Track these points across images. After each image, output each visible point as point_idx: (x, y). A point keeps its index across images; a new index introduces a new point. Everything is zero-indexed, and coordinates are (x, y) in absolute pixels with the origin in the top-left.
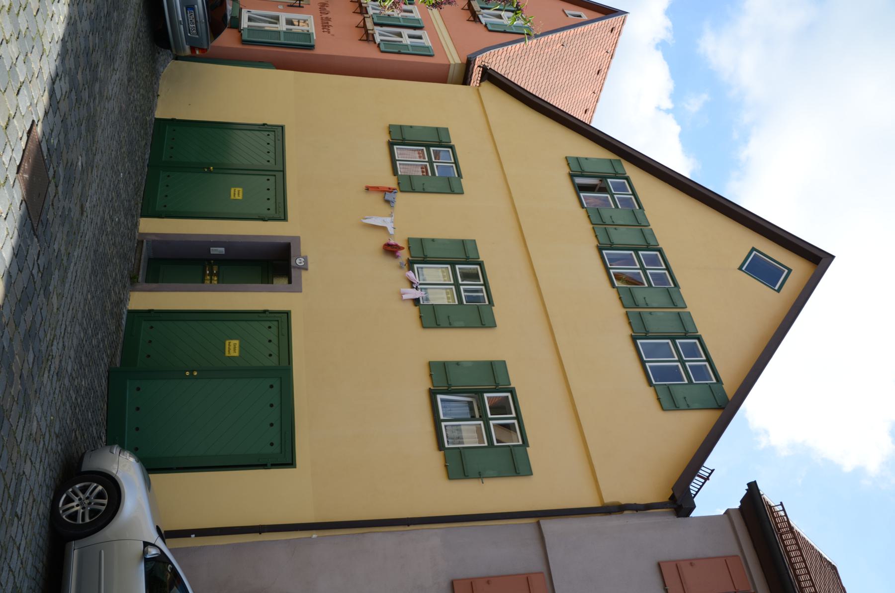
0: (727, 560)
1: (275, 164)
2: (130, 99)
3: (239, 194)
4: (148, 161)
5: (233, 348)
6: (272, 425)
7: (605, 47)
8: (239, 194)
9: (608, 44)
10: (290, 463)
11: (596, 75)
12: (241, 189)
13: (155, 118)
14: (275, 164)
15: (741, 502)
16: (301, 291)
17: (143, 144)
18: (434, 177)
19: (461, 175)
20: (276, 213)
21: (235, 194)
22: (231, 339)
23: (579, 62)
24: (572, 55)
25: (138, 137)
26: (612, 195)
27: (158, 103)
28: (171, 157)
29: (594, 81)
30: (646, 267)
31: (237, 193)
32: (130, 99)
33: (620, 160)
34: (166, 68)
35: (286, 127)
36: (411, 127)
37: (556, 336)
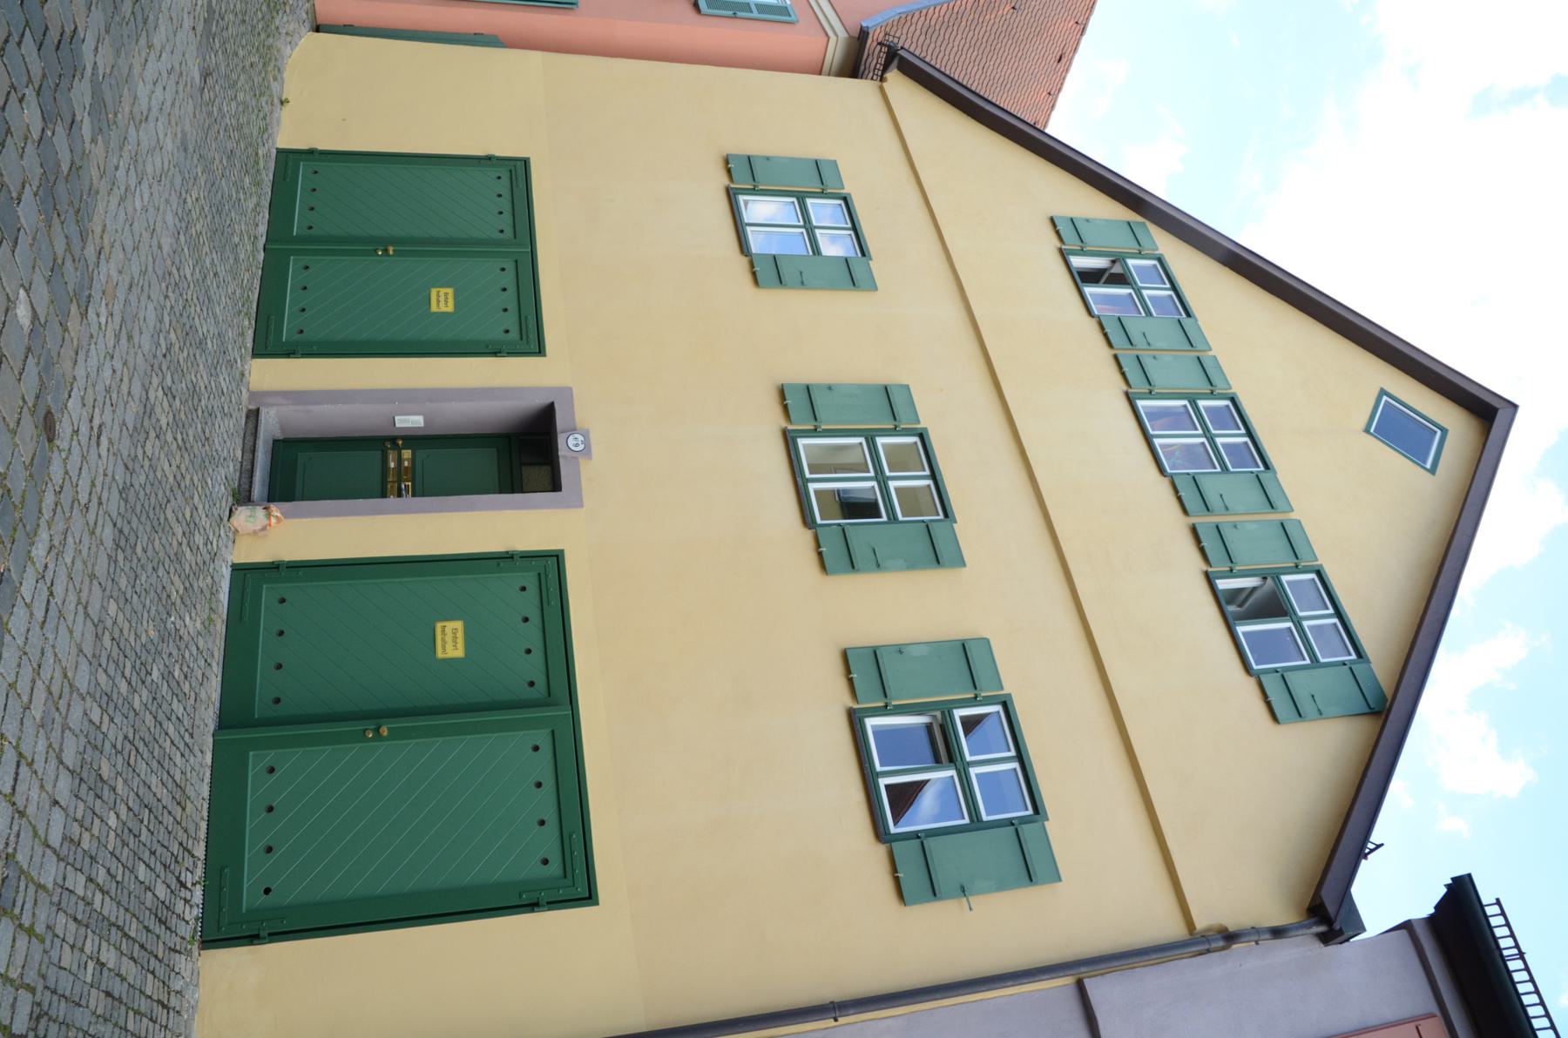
0: (1420, 1028)
1: (515, 237)
2: (210, 114)
3: (446, 302)
4: (264, 237)
5: (451, 641)
6: (539, 785)
7: (1074, 15)
8: (446, 302)
9: (1081, 9)
10: (589, 897)
11: (1056, 63)
12: (450, 291)
13: (277, 149)
14: (515, 237)
15: (1436, 907)
16: (581, 505)
17: (251, 206)
18: (817, 257)
19: (869, 253)
20: (522, 339)
21: (438, 301)
22: (447, 620)
23: (1035, 39)
24: (1025, 26)
25: (237, 192)
26: (1138, 291)
27: (282, 119)
28: (311, 228)
29: (1052, 73)
30: (1214, 432)
31: (442, 298)
32: (210, 114)
33: (1144, 223)
34: (297, 48)
35: (531, 161)
36: (768, 158)
37: (1076, 581)
